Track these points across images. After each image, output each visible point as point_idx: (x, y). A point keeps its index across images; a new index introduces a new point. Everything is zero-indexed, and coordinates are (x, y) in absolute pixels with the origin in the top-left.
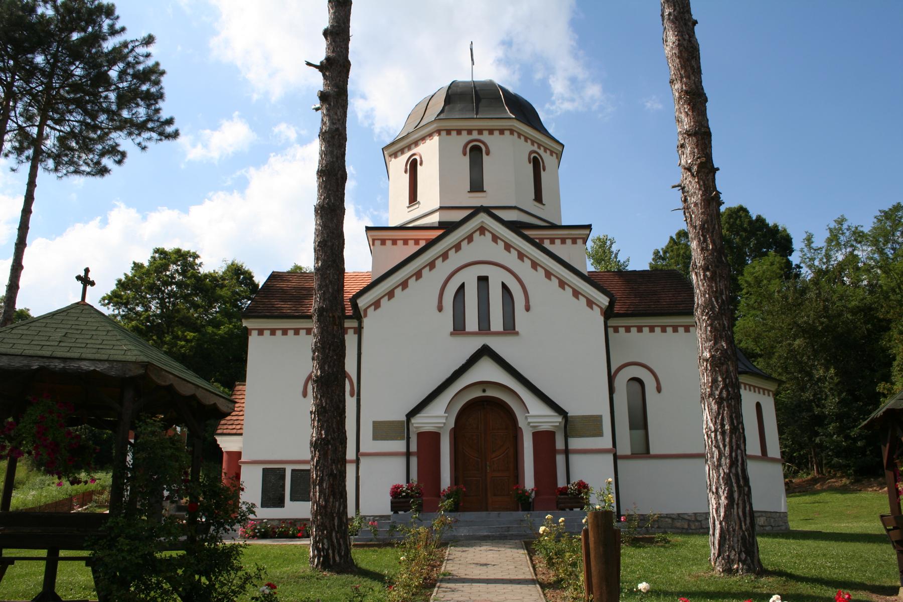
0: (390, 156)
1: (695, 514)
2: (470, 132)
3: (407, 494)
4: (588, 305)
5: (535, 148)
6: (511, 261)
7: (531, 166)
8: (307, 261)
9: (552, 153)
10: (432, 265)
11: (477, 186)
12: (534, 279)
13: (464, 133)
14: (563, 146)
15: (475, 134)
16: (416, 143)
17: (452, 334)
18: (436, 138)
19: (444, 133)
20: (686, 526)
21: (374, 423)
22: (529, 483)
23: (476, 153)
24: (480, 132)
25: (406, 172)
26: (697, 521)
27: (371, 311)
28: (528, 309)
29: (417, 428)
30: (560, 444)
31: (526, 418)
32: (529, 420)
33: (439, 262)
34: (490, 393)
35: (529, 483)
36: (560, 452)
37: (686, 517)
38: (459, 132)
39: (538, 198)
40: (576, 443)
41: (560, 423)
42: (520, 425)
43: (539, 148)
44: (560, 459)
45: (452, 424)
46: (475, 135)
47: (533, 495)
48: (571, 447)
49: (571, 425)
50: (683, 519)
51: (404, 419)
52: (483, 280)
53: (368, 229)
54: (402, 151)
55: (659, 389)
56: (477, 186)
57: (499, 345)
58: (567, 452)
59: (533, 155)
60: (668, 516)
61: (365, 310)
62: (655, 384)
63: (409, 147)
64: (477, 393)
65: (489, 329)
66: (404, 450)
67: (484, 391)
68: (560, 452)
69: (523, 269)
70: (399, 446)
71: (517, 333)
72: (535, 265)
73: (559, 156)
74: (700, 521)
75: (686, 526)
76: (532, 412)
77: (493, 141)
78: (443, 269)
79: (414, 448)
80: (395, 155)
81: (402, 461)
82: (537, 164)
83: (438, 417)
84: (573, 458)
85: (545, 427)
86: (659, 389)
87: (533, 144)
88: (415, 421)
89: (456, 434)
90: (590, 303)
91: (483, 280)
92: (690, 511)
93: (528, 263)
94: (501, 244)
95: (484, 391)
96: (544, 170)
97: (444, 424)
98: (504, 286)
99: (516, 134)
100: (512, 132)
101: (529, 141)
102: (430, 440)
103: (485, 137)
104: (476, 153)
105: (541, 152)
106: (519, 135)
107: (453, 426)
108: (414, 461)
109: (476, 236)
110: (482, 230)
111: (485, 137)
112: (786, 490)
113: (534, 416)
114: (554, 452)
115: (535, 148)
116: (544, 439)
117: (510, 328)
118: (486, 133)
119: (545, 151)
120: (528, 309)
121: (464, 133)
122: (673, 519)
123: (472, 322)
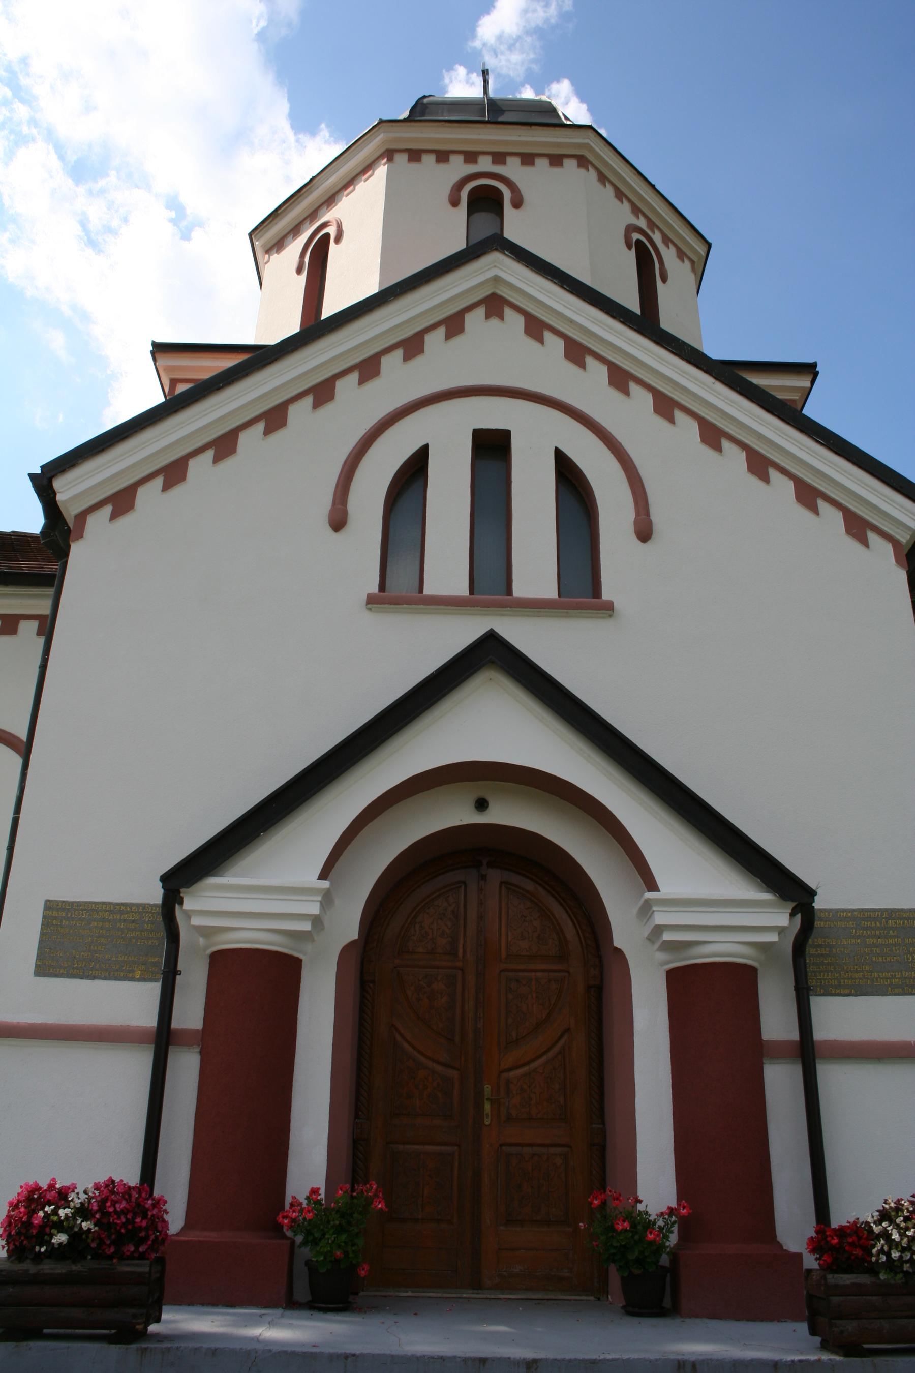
0: (268, 251)
2: (471, 157)
3: (77, 1236)
4: (849, 531)
5: (642, 223)
6: (589, 388)
7: (631, 257)
9: (681, 255)
10: (322, 393)
12: (667, 451)
14: (709, 246)
16: (331, 200)
17: (371, 600)
18: (382, 170)
19: (401, 159)
21: (50, 906)
22: (655, 1184)
25: (299, 271)
27: (98, 522)
28: (644, 532)
29: (207, 932)
30: (776, 1021)
31: (646, 909)
32: (661, 918)
33: (347, 387)
34: (509, 813)
35: (655, 1184)
36: (779, 1051)
40: (840, 1018)
41: (781, 930)
42: (618, 941)
44: (780, 1082)
45: (347, 925)
47: (673, 1239)
48: (820, 1033)
49: (818, 951)
51: (155, 894)
52: (492, 448)
53: (159, 349)
54: (295, 231)
57: (541, 641)
58: (807, 1052)
61: (82, 517)
63: (313, 215)
64: (452, 813)
65: (509, 592)
66: (149, 1019)
67: (481, 805)
68: (779, 1051)
70: (131, 1002)
71: (608, 608)
72: (665, 406)
76: (668, 886)
78: (358, 405)
79: (190, 1013)
80: (278, 245)
81: (141, 1063)
83: (292, 896)
84: (834, 1078)
85: (722, 948)
88: (203, 904)
89: (368, 968)
91: (492, 448)
93: (642, 399)
94: (555, 345)
95: (481, 805)
96: (664, 279)
97: (317, 921)
100: (583, 162)
102: (258, 984)
103: (512, 169)
105: (657, 238)
107: (352, 933)
108: (186, 1068)
109: (475, 320)
110: (495, 305)
111: (512, 169)
112: (37, 966)
113: (679, 904)
114: (754, 1052)
116: (710, 996)
117: (582, 583)
120: (644, 532)
123: (447, 560)
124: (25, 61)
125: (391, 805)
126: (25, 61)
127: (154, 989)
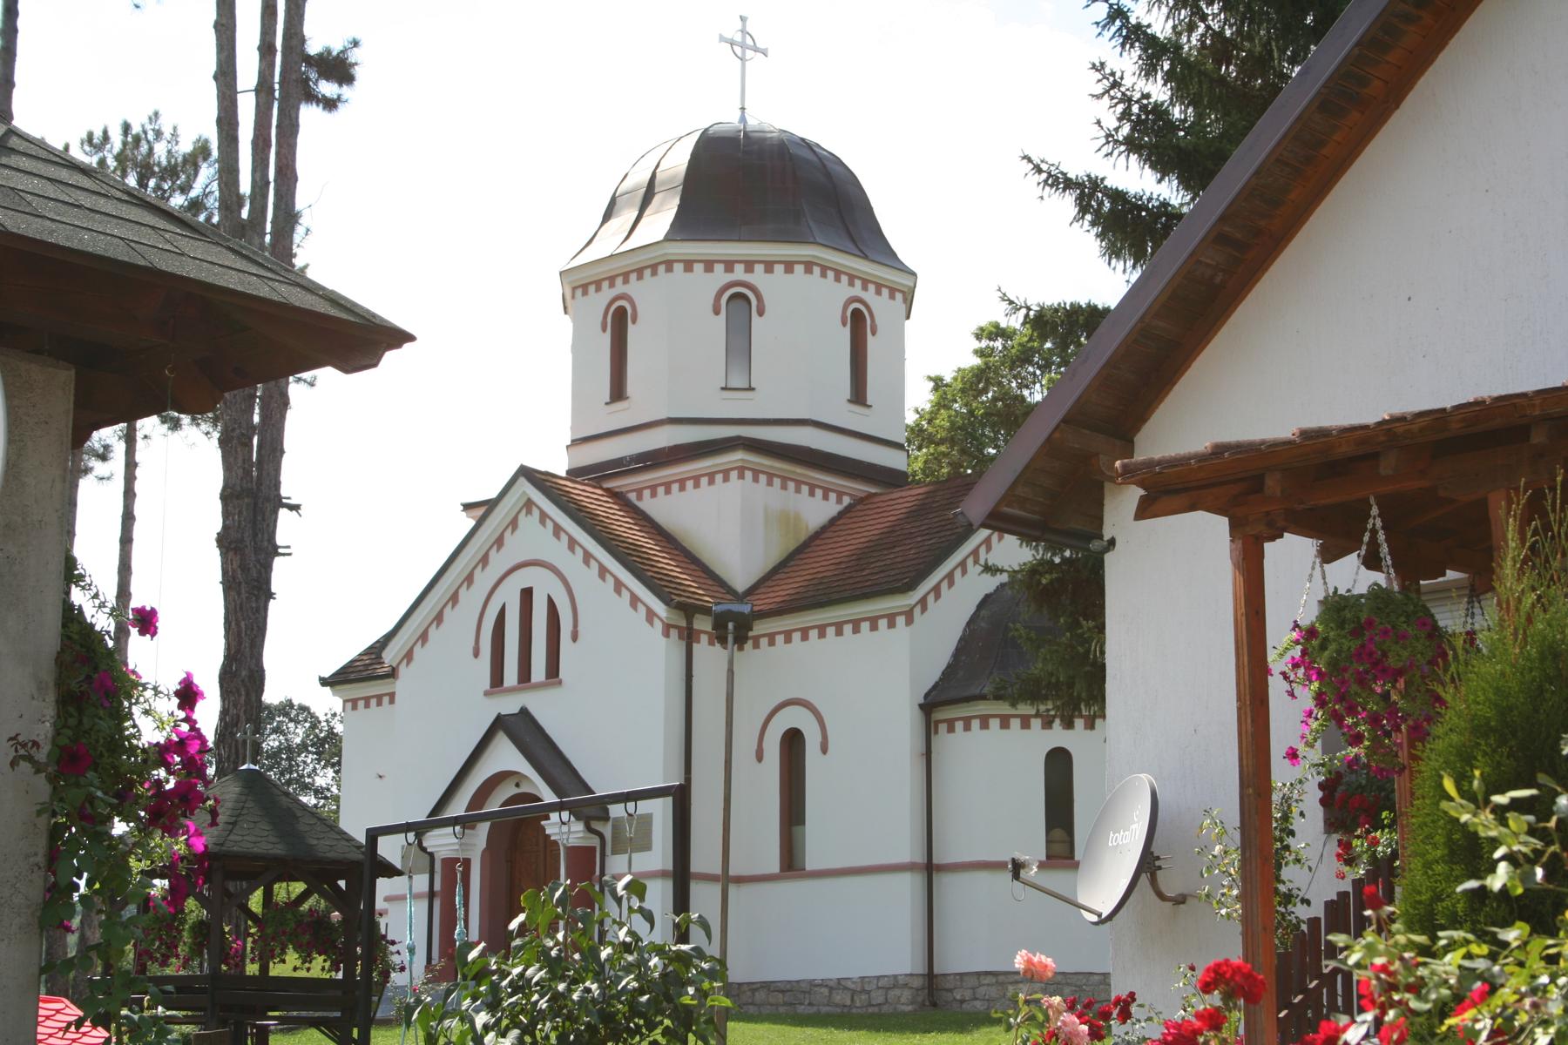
2: (729, 266)
5: (857, 290)
7: (845, 333)
12: (584, 579)
13: (719, 268)
14: (914, 274)
15: (739, 269)
17: (486, 694)
20: (848, 1002)
23: (740, 306)
24: (749, 266)
26: (863, 991)
27: (402, 670)
34: (524, 789)
37: (849, 985)
38: (709, 266)
39: (859, 395)
43: (865, 288)
46: (620, 288)
50: (846, 988)
52: (527, 594)
62: (819, 738)
64: (507, 791)
73: (909, 298)
74: (868, 992)
75: (848, 1002)
81: (425, 904)
82: (859, 323)
86: (824, 750)
90: (651, 615)
91: (527, 594)
92: (855, 974)
95: (517, 785)
98: (551, 604)
103: (758, 277)
104: (740, 306)
105: (869, 296)
111: (758, 277)
115: (857, 290)
118: (759, 268)
120: (575, 637)
121: (719, 268)
122: (831, 989)
127: (426, 877)
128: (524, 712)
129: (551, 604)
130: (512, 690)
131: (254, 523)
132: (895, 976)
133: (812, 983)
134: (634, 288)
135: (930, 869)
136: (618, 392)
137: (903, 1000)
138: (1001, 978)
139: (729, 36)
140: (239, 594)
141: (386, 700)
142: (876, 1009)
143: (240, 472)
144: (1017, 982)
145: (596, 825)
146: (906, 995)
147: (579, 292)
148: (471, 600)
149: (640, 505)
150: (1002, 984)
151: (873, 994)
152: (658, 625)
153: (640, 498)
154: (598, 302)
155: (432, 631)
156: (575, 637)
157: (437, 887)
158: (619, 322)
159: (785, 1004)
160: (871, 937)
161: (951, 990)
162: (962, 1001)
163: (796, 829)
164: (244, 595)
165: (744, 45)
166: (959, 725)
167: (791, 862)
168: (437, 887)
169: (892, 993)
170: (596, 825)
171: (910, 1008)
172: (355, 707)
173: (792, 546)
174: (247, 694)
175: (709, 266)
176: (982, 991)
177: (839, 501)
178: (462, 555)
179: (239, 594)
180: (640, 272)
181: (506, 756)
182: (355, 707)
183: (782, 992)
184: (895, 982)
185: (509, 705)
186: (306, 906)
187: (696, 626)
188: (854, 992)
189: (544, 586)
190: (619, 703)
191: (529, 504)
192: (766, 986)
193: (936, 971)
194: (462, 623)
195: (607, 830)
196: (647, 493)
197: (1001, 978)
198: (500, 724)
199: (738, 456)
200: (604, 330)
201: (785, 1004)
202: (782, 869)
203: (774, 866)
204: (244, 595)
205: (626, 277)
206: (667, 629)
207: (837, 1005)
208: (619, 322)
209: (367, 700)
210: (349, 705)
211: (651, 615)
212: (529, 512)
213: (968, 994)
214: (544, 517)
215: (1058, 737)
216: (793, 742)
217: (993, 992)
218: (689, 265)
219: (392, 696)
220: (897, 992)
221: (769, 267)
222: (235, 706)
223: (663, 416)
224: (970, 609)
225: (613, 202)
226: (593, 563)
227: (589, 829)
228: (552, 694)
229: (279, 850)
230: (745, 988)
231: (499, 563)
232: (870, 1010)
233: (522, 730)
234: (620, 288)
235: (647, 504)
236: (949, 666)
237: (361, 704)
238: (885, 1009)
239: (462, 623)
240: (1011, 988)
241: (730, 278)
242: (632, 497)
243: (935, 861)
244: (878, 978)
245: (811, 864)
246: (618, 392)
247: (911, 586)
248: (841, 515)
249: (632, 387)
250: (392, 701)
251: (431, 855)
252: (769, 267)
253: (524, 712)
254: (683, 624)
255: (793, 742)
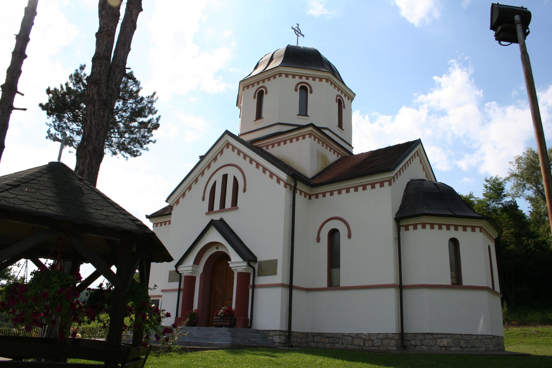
1: (369, 334)
2: (301, 77)
8: (341, 285)
11: (303, 111)
13: (297, 77)
17: (206, 214)
20: (362, 344)
23: (304, 90)
24: (307, 78)
34: (221, 249)
38: (294, 76)
39: (340, 125)
43: (342, 93)
46: (261, 84)
50: (360, 338)
51: (175, 269)
52: (225, 177)
55: (349, 236)
56: (303, 111)
59: (339, 98)
60: (349, 335)
62: (347, 232)
64: (213, 250)
66: (177, 287)
67: (217, 248)
69: (244, 164)
74: (373, 340)
75: (362, 344)
77: (315, 84)
81: (177, 293)
86: (349, 236)
87: (338, 91)
88: (181, 269)
90: (279, 180)
91: (225, 177)
92: (366, 332)
95: (217, 248)
96: (344, 108)
98: (235, 180)
99: (329, 82)
100: (327, 80)
101: (337, 88)
102: (190, 280)
103: (310, 81)
104: (304, 90)
105: (343, 96)
106: (331, 83)
115: (339, 93)
118: (311, 79)
119: (345, 97)
120: (244, 191)
121: (297, 77)
122: (353, 338)
123: (217, 206)
124: (448, 115)
125: (203, 254)
126: (448, 115)
127: (178, 283)
128: (222, 220)
129: (235, 180)
130: (217, 212)
131: (109, 75)
132: (387, 334)
133: (343, 335)
134: (267, 84)
135: (401, 287)
136: (259, 116)
137: (391, 345)
138: (435, 336)
139: (294, 27)
140: (94, 106)
141: (168, 223)
142: (377, 348)
143: (104, 48)
144: (441, 338)
145: (252, 264)
146: (393, 343)
147: (246, 88)
148: (203, 180)
149: (268, 151)
150: (435, 339)
151: (375, 341)
152: (282, 183)
153: (267, 148)
154: (253, 90)
155: (187, 193)
156: (244, 191)
157: (182, 287)
158: (260, 95)
159: (329, 343)
160: (375, 317)
161: (409, 341)
162: (415, 346)
163: (334, 270)
164: (97, 107)
165: (298, 32)
166: (411, 228)
167: (333, 284)
168: (182, 287)
169: (385, 342)
170: (252, 264)
171: (395, 348)
172: (157, 226)
173: (325, 167)
174: (91, 159)
175: (294, 76)
176: (426, 341)
177: (338, 156)
178: (199, 167)
179: (94, 106)
180: (269, 79)
181: (214, 236)
182: (157, 226)
183: (328, 337)
184: (387, 336)
185: (216, 217)
186: (94, 286)
187: (297, 187)
188: (364, 340)
189: (232, 172)
190: (263, 216)
191: (228, 145)
192: (321, 335)
193: (405, 332)
194: (198, 189)
195: (256, 266)
196: (270, 147)
197: (435, 336)
198: (212, 223)
199: (310, 128)
200: (255, 98)
201: (329, 343)
202: (328, 286)
203: (325, 285)
204: (97, 107)
205: (263, 81)
206: (286, 185)
207: (356, 345)
208: (260, 95)
209: (161, 223)
210: (155, 225)
211: (279, 180)
212: (228, 147)
213: (419, 343)
214: (234, 148)
215: (453, 234)
216: (334, 234)
217: (432, 342)
218: (287, 75)
219: (170, 222)
220: (388, 341)
221: (314, 79)
222: (83, 164)
223: (277, 122)
224: (404, 187)
225: (258, 64)
226: (260, 167)
227: (249, 265)
228: (234, 213)
229: (53, 210)
230: (310, 335)
231: (214, 166)
232: (373, 348)
233: (222, 226)
234: (261, 84)
235: (271, 150)
236: (401, 205)
237: (159, 225)
238: (381, 348)
239: (198, 189)
240: (439, 341)
241: (301, 81)
242: (264, 148)
243: (404, 284)
244: (378, 334)
245: (465, 283)
246: (259, 116)
247: (393, 169)
248: (338, 160)
249: (264, 114)
250: (170, 224)
251: (180, 274)
252: (314, 79)
253: (222, 220)
254: (293, 184)
255: (334, 234)
